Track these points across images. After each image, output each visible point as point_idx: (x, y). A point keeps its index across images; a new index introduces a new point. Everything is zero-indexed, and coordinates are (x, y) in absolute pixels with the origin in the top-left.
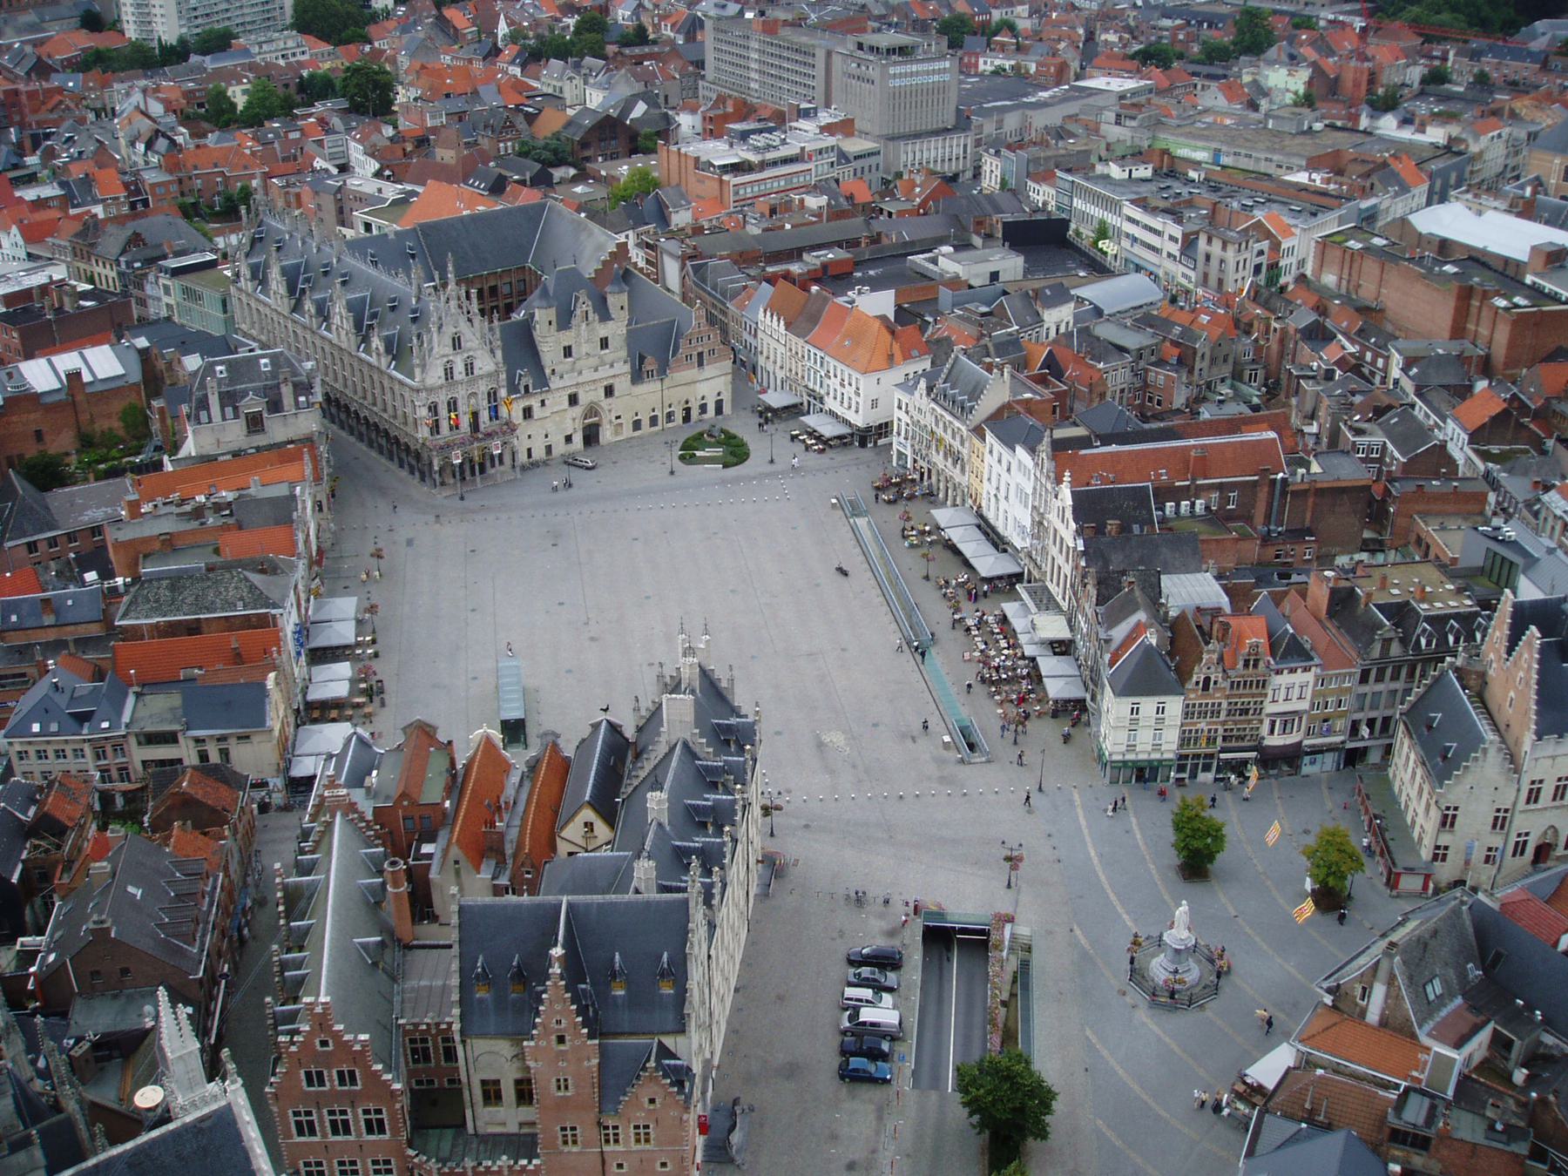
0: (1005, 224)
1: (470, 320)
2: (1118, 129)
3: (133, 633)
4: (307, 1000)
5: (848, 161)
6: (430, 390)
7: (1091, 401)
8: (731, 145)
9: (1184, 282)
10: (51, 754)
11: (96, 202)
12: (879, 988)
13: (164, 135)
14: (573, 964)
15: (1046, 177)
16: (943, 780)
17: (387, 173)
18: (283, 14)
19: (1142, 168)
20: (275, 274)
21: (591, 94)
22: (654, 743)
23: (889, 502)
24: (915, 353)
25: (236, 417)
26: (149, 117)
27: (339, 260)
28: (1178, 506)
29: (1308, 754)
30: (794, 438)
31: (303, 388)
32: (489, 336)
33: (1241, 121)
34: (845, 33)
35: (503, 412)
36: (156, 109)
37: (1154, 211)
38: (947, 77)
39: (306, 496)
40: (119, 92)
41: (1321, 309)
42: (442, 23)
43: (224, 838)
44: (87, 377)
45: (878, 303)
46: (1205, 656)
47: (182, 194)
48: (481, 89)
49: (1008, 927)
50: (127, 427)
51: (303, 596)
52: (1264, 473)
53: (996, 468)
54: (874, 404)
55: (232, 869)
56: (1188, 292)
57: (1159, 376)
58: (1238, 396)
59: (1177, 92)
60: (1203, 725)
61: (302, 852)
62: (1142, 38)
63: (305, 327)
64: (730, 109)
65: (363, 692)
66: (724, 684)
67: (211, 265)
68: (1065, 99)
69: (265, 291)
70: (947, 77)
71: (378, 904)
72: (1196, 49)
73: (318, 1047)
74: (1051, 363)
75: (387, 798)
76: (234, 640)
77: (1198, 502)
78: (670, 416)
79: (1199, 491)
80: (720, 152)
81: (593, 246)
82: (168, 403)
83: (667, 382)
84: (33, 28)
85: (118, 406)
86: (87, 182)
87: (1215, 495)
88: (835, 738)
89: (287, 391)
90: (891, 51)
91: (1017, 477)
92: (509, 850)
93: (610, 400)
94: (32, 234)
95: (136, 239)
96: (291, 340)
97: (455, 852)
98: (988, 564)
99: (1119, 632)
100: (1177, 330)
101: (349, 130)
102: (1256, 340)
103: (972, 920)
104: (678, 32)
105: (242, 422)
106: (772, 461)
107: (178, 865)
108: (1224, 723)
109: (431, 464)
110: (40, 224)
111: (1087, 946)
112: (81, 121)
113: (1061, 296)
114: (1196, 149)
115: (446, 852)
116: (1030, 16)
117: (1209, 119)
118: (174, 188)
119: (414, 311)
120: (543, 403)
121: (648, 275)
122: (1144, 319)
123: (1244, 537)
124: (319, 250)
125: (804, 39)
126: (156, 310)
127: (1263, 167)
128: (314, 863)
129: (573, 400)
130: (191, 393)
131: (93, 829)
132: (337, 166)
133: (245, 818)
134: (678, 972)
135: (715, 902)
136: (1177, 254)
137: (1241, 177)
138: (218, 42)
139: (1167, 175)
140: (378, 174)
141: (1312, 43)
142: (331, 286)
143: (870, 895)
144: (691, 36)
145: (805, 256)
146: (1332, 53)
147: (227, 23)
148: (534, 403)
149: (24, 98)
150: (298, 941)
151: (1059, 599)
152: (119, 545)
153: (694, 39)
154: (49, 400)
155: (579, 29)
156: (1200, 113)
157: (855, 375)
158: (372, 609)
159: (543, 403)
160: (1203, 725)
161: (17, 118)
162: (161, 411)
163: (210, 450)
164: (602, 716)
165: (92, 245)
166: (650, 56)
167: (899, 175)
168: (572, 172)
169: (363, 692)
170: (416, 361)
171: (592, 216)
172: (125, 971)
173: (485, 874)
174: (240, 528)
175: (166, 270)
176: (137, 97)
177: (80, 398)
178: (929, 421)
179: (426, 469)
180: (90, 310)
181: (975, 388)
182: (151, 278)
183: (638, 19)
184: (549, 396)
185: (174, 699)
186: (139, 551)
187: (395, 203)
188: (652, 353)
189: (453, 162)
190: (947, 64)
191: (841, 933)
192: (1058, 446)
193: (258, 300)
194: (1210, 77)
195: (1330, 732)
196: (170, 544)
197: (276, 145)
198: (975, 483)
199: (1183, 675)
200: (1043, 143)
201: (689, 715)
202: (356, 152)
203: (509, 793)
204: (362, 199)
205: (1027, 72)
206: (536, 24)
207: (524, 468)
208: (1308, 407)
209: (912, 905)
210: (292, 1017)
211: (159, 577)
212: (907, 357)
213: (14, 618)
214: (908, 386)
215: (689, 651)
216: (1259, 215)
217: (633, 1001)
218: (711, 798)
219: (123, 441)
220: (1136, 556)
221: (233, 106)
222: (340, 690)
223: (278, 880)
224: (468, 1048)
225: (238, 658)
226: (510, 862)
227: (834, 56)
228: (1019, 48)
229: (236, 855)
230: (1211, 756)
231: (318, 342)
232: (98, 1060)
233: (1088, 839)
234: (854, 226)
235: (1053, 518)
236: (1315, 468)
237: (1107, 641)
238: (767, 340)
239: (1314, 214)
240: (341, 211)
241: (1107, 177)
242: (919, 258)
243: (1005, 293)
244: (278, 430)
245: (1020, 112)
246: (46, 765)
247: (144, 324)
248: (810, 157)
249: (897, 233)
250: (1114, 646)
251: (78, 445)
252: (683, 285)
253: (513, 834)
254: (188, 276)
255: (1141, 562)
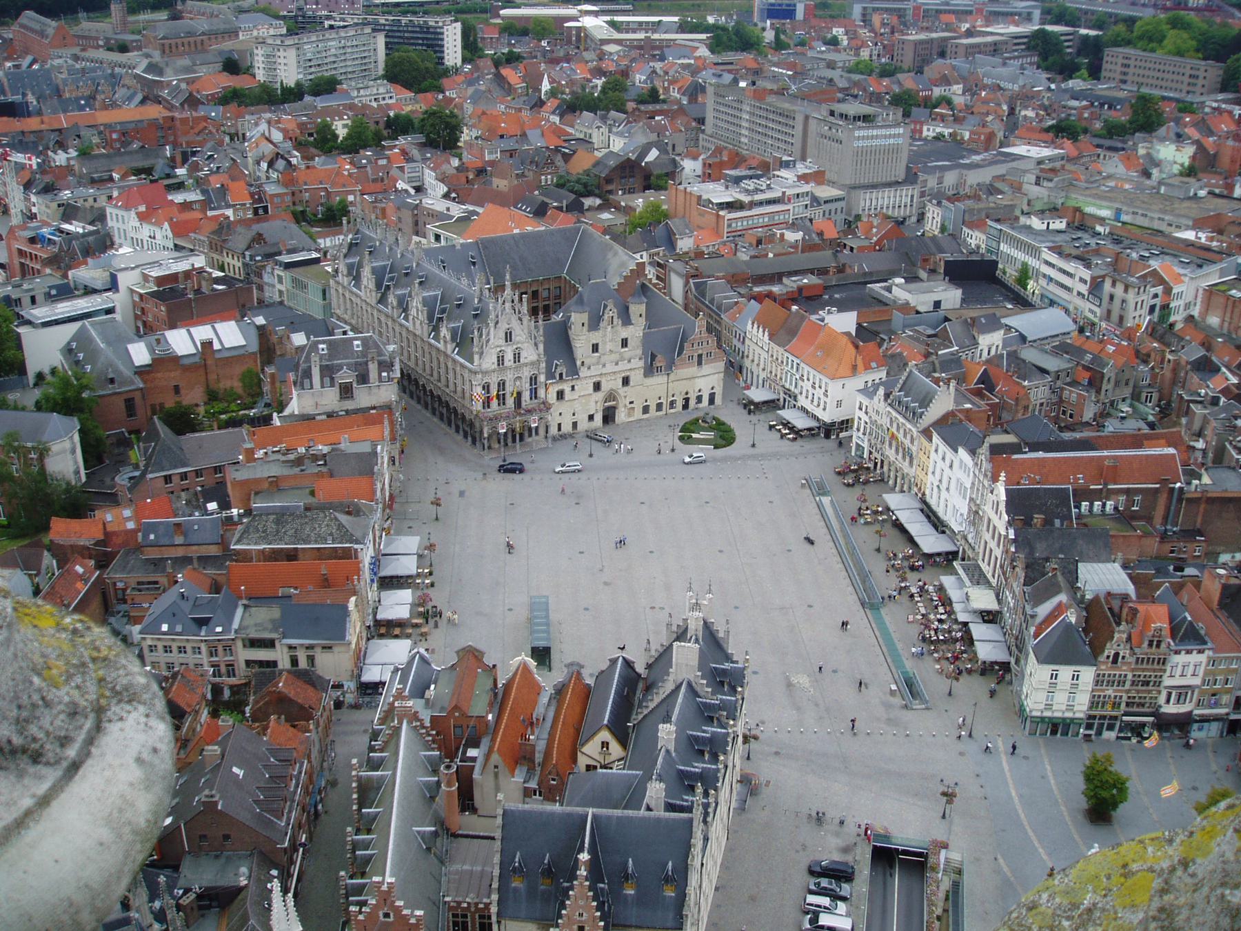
0: (946, 262)
1: (520, 319)
2: (1037, 188)
3: (244, 556)
4: (376, 879)
5: (819, 204)
6: (485, 373)
7: (1017, 411)
8: (727, 187)
9: (1091, 316)
10: (175, 649)
11: (228, 206)
12: (836, 897)
13: (282, 157)
14: (594, 865)
15: (978, 225)
16: (889, 721)
17: (453, 195)
18: (376, 67)
19: (1057, 222)
20: (366, 273)
21: (611, 141)
22: (664, 681)
23: (848, 485)
24: (874, 365)
25: (332, 385)
26: (271, 142)
27: (418, 264)
28: (1091, 505)
29: (1197, 721)
30: (771, 427)
31: (386, 366)
32: (534, 332)
33: (1139, 187)
34: (820, 102)
35: (541, 393)
36: (277, 136)
37: (1067, 257)
38: (900, 141)
39: (384, 452)
40: (249, 122)
41: (1207, 345)
42: (500, 79)
43: (309, 731)
44: (217, 346)
45: (843, 322)
46: (1116, 636)
47: (294, 204)
48: (528, 132)
49: (943, 852)
50: (244, 386)
51: (378, 534)
52: (1164, 482)
53: (940, 464)
54: (839, 404)
55: (313, 756)
56: (1093, 324)
57: (1072, 394)
58: (1137, 414)
59: (1084, 160)
60: (1110, 692)
61: (372, 749)
62: (1054, 115)
63: (387, 316)
64: (725, 158)
65: (421, 615)
66: (721, 635)
67: (316, 261)
68: (993, 163)
69: (358, 285)
70: (900, 141)
71: (432, 798)
72: (1098, 125)
73: (381, 918)
74: (985, 379)
75: (442, 709)
76: (324, 568)
77: (1096, 503)
78: (672, 404)
79: (1110, 494)
80: (717, 193)
81: (622, 261)
82: (278, 369)
83: (672, 377)
84: (187, 70)
85: (239, 370)
86: (223, 189)
87: (1122, 498)
88: (802, 680)
89: (373, 368)
90: (857, 118)
91: (958, 473)
92: (539, 757)
93: (626, 388)
94: (179, 230)
95: (259, 238)
96: (376, 325)
97: (495, 758)
98: (930, 542)
99: (1044, 610)
100: (1089, 357)
101: (425, 160)
102: (1153, 368)
103: (913, 844)
104: (683, 94)
105: (336, 389)
106: (753, 445)
107: (273, 752)
108: (1128, 691)
109: (481, 432)
110: (186, 222)
111: (1009, 874)
112: (221, 143)
113: (993, 324)
114: (1100, 207)
115: (488, 757)
116: (964, 93)
117: (1112, 184)
118: (288, 199)
119: (476, 309)
120: (573, 387)
121: (660, 289)
122: (1063, 348)
123: (1146, 535)
124: (402, 255)
125: (786, 106)
126: (272, 295)
127: (1156, 225)
128: (382, 759)
129: (597, 387)
130: (298, 364)
131: (204, 715)
132: (414, 188)
133: (325, 714)
134: (680, 878)
135: (710, 819)
136: (1086, 293)
137: (1138, 231)
138: (326, 86)
139: (1078, 228)
140: (446, 196)
141: (1195, 125)
142: (411, 284)
143: (828, 816)
144: (693, 98)
145: (785, 280)
146: (1211, 133)
147: (334, 72)
148: (566, 387)
149: (178, 123)
150: (366, 825)
151: (989, 576)
152: (237, 484)
153: (696, 99)
154: (186, 362)
155: (604, 90)
156: (1104, 178)
157: (825, 380)
158: (431, 547)
159: (573, 387)
160: (1110, 692)
161: (171, 138)
162: (273, 376)
163: (310, 410)
164: (619, 654)
165: (224, 241)
166: (660, 113)
167: (858, 217)
168: (598, 201)
169: (421, 615)
170: (476, 349)
171: (615, 238)
172: (226, 837)
173: (519, 778)
174: (331, 476)
175: (281, 264)
176: (263, 127)
177: (209, 362)
178: (885, 421)
179: (477, 435)
180: (222, 293)
181: (925, 397)
182: (269, 269)
183: (652, 82)
184: (578, 382)
185: (275, 612)
186: (252, 489)
187: (460, 220)
188: (662, 354)
189: (506, 189)
190: (901, 131)
191: (804, 847)
192: (996, 450)
193: (351, 292)
194: (1110, 149)
195: (1216, 705)
196: (275, 485)
197: (369, 169)
198: (921, 475)
199: (1096, 650)
200: (976, 197)
201: (694, 661)
202: (429, 177)
203: (539, 710)
204: (435, 216)
205: (962, 138)
206: (572, 82)
207: (554, 439)
208: (1196, 426)
209: (863, 828)
210: (359, 890)
211: (267, 512)
212: (867, 367)
213: (152, 537)
214: (868, 391)
215: (696, 606)
216: (1155, 264)
217: (640, 900)
218: (710, 730)
219: (240, 398)
220: (1057, 545)
221: (336, 136)
222: (403, 613)
223: (354, 773)
224: (502, 927)
225: (326, 583)
226: (538, 769)
227: (810, 120)
228: (957, 120)
229: (317, 746)
230: (1116, 718)
231: (397, 328)
232: (200, 908)
233: (1010, 782)
234: (824, 257)
235: (988, 510)
236: (1206, 480)
237: (1033, 617)
238: (753, 346)
239: (1200, 266)
240: (416, 223)
241: (1030, 227)
242: (877, 287)
243: (947, 319)
244: (364, 398)
245: (957, 171)
246: (175, 657)
247: (262, 305)
248: (789, 200)
249: (860, 266)
250: (1039, 620)
251: (206, 399)
252: (686, 297)
253: (541, 746)
254: (297, 270)
255: (1061, 551)
